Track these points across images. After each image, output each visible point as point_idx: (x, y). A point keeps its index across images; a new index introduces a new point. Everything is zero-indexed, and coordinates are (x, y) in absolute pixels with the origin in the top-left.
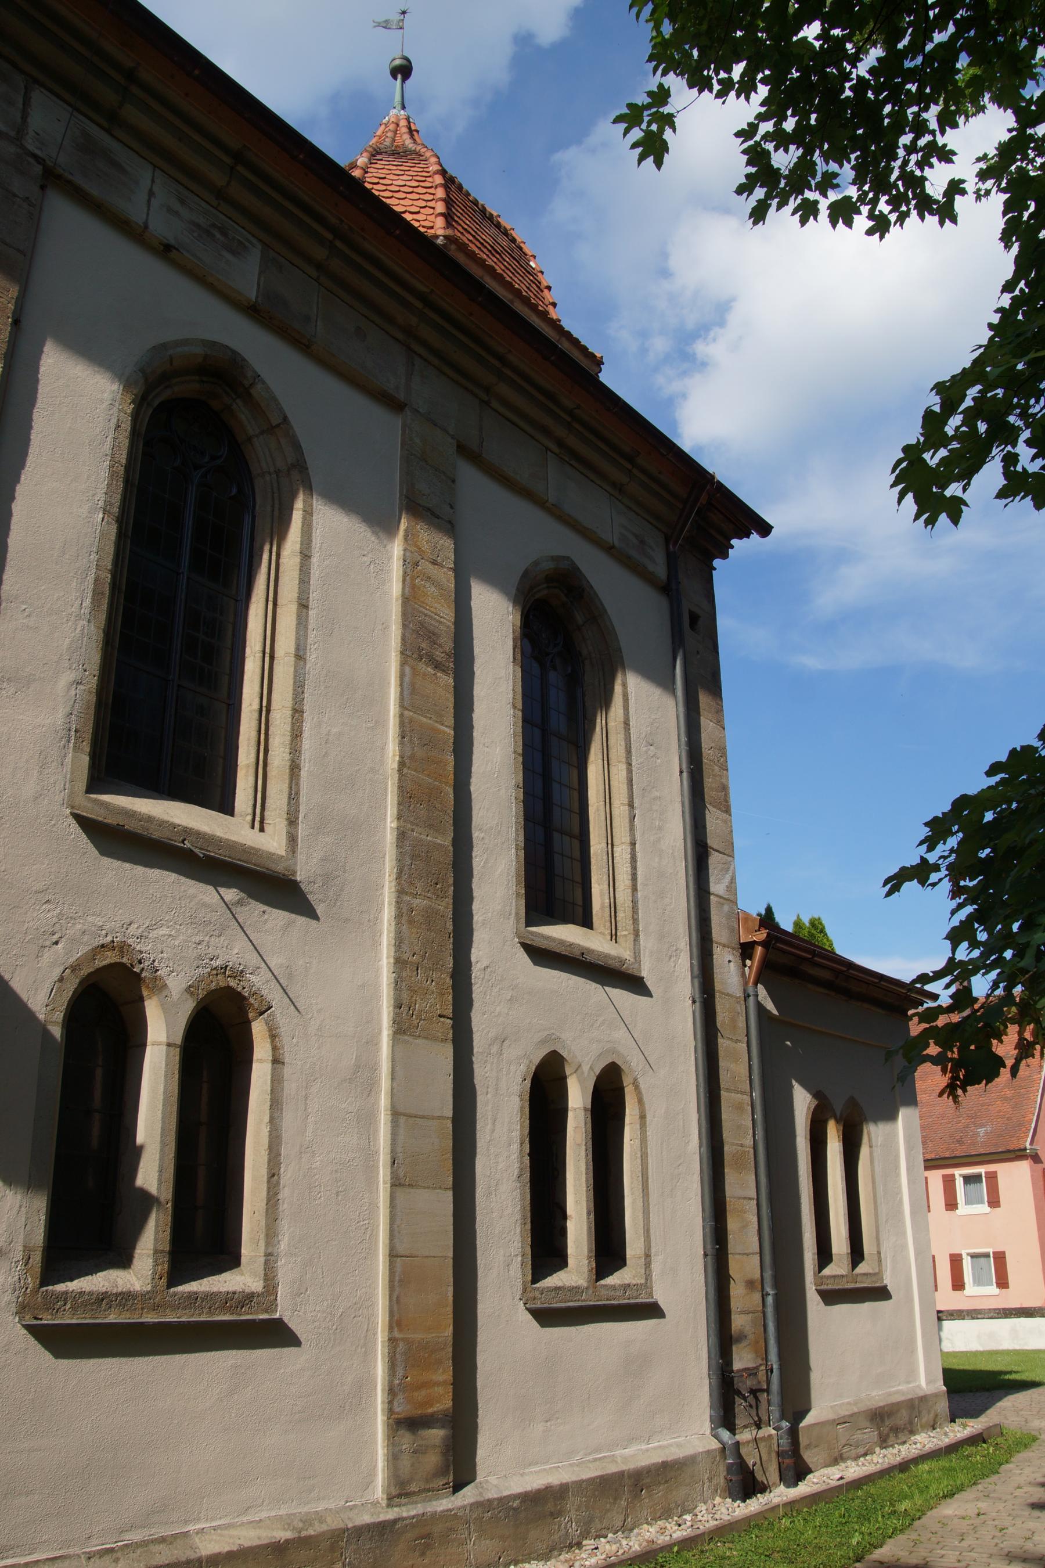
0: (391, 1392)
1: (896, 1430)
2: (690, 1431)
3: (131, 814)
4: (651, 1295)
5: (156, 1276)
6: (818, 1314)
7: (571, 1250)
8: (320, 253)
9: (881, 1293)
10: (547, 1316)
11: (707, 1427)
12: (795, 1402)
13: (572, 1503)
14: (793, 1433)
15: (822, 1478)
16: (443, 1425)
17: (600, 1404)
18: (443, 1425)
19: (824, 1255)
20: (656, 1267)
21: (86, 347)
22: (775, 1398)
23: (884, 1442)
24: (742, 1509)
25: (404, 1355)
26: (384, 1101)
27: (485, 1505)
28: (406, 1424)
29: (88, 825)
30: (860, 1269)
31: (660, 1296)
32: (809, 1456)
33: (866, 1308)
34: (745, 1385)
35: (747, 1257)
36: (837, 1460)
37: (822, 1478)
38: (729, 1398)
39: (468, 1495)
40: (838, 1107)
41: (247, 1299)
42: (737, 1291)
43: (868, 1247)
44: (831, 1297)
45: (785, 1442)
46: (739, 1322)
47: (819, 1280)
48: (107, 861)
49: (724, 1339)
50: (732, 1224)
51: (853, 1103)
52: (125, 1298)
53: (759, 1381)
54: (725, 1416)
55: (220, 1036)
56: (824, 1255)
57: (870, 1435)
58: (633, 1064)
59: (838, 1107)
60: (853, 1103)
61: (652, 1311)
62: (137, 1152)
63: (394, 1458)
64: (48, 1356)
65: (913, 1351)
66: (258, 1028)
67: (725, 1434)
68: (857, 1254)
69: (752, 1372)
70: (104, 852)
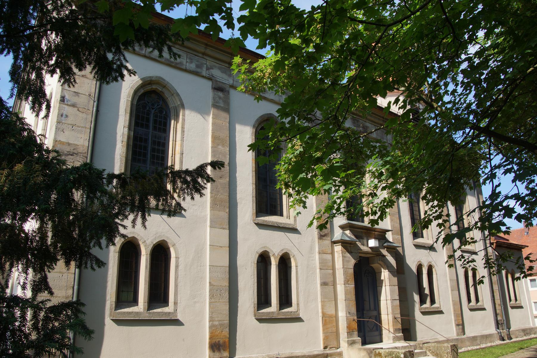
0: (455, 320)
1: (527, 333)
2: (492, 329)
3: (264, 221)
4: (177, 316)
5: (144, 308)
6: (511, 311)
7: (472, 299)
8: (202, 49)
9: (521, 307)
10: (471, 310)
11: (494, 329)
12: (509, 327)
13: (478, 338)
14: (509, 331)
15: (514, 340)
16: (461, 326)
17: (481, 324)
18: (461, 326)
19: (510, 300)
20: (484, 302)
21: (244, 123)
22: (505, 325)
23: (525, 335)
24: (503, 342)
25: (456, 315)
26: (448, 278)
27: (468, 337)
28: (458, 325)
29: (258, 224)
30: (478, 304)
31: (485, 307)
32: (512, 336)
33: (519, 310)
34: (500, 322)
35: (498, 301)
36: (517, 338)
37: (514, 340)
38: (498, 324)
39: (465, 336)
40: (510, 271)
41: (438, 308)
42: (497, 306)
43: (480, 299)
44: (512, 308)
45: (508, 333)
46: (498, 311)
47: (510, 304)
48: (261, 230)
49: (496, 315)
50: (495, 294)
51: (513, 270)
52: (137, 313)
53: (502, 322)
54: (498, 328)
55: (285, 262)
56: (510, 300)
57: (522, 334)
58: (433, 263)
59: (510, 271)
60: (513, 270)
61: (484, 309)
62: (425, 288)
63: (456, 330)
64: (116, 325)
65: (529, 318)
66: (433, 270)
67: (498, 330)
68: (516, 300)
69: (501, 320)
70: (260, 229)
